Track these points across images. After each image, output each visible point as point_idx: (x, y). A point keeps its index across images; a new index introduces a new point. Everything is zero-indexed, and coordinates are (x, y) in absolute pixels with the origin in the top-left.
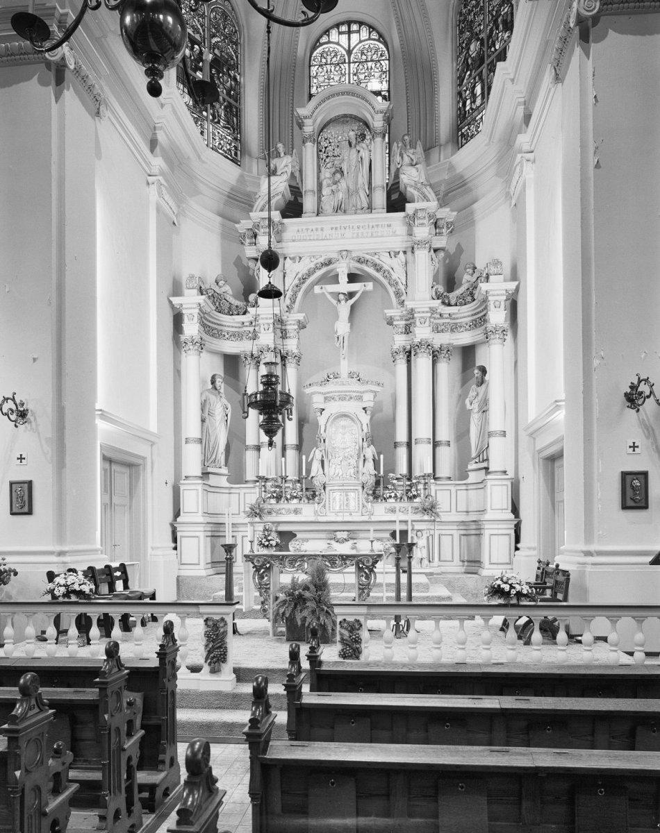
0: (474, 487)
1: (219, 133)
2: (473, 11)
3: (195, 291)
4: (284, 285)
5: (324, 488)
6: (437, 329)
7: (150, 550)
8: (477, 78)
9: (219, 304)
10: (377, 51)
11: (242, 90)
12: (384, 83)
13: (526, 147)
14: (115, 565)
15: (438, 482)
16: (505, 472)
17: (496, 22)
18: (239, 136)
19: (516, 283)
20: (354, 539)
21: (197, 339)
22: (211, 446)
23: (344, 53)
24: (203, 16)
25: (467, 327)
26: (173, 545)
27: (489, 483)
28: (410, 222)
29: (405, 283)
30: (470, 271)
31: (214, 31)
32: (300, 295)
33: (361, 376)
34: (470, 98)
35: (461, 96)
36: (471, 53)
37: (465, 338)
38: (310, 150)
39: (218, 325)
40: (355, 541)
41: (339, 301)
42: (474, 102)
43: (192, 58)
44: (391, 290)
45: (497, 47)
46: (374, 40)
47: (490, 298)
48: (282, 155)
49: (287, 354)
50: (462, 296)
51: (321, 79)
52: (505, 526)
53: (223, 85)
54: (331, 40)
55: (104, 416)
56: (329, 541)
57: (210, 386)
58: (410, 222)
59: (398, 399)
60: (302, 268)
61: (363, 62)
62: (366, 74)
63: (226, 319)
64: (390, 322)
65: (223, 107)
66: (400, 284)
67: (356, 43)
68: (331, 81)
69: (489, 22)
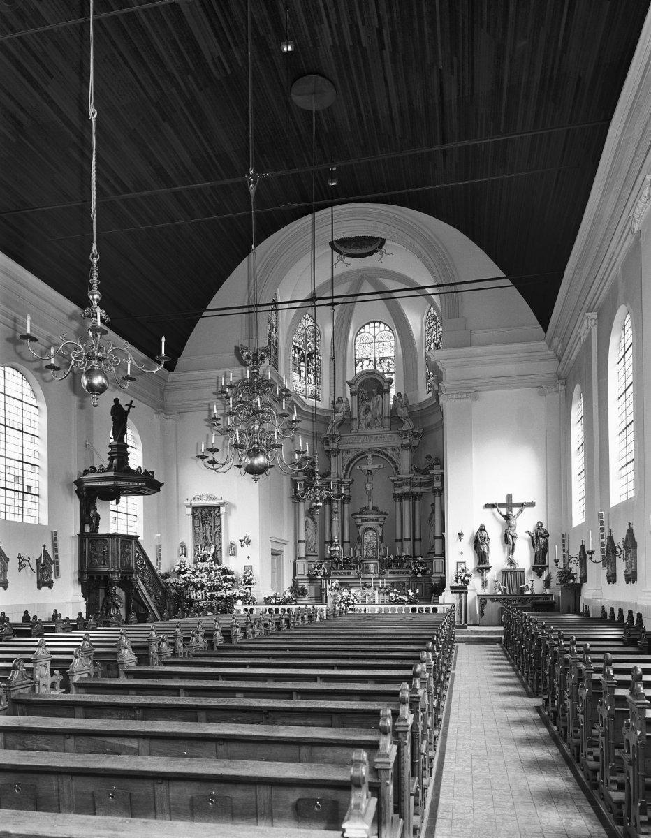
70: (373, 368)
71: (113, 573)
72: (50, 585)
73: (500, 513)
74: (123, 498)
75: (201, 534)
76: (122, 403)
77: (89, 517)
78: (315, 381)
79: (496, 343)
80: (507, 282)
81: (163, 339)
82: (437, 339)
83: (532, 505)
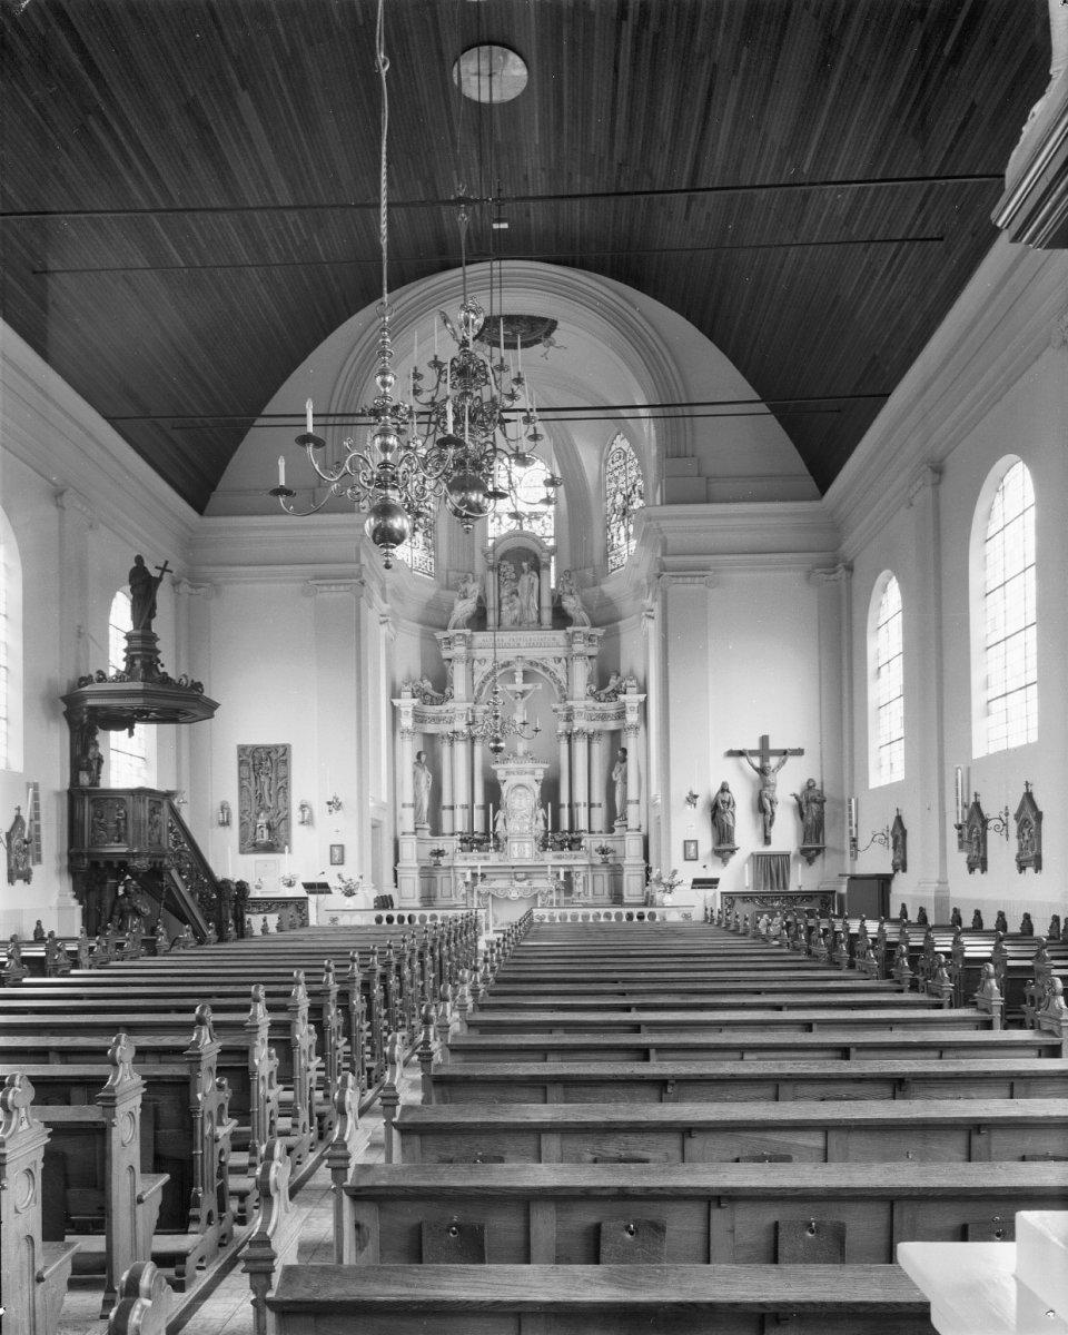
28: (570, 639)
37: (612, 725)
50: (607, 695)
70: (518, 528)
71: (138, 855)
72: (27, 878)
73: (752, 765)
74: (139, 727)
75: (252, 792)
76: (149, 565)
77: (84, 759)
78: (425, 544)
79: (744, 500)
80: (763, 407)
81: (282, 463)
82: (627, 487)
83: (799, 752)
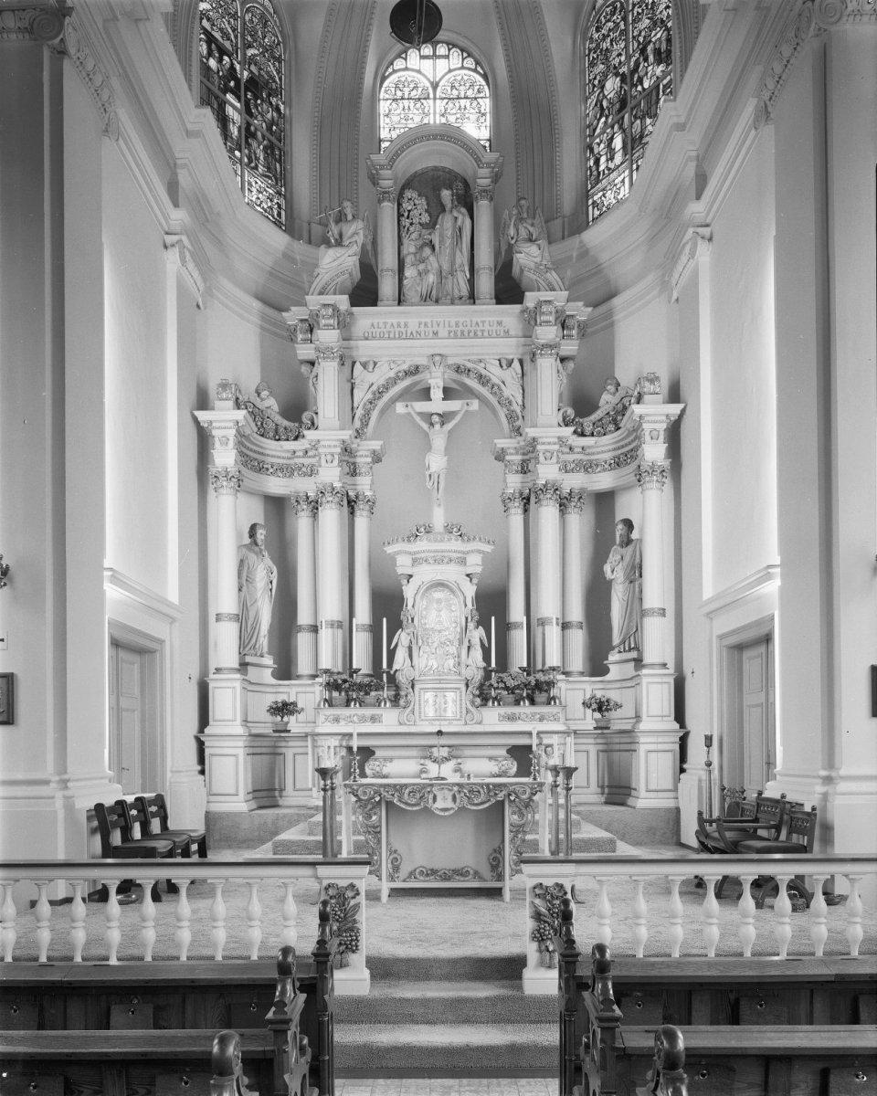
0: (618, 685)
1: (256, 183)
2: (609, 36)
3: (231, 404)
4: (353, 402)
5: (413, 687)
6: (565, 469)
7: (169, 775)
8: (616, 127)
9: (262, 424)
10: (472, 86)
11: (288, 127)
12: (483, 128)
13: (700, 218)
14: (130, 799)
15: (571, 679)
16: (664, 665)
17: (643, 51)
18: (283, 189)
19: (681, 406)
20: (459, 757)
21: (233, 470)
22: (249, 625)
23: (428, 85)
24: (235, 16)
25: (607, 466)
26: (199, 768)
27: (645, 681)
28: (531, 319)
29: (520, 403)
30: (611, 388)
31: (249, 39)
32: (375, 415)
33: (463, 530)
34: (606, 154)
35: (592, 150)
36: (606, 93)
37: (604, 481)
38: (388, 210)
39: (259, 453)
40: (459, 760)
41: (432, 424)
42: (612, 159)
43: (221, 74)
44: (502, 413)
45: (646, 85)
46: (469, 69)
47: (645, 426)
48: (350, 217)
49: (357, 497)
51: (396, 119)
52: (667, 739)
53: (263, 116)
54: (409, 66)
55: (116, 579)
56: (422, 761)
57: (247, 540)
58: (531, 319)
59: (511, 564)
60: (379, 377)
61: (453, 99)
62: (458, 116)
63: (271, 446)
64: (500, 456)
65: (262, 147)
66: (514, 404)
67: (443, 73)
68: (410, 121)
69: (634, 51)
